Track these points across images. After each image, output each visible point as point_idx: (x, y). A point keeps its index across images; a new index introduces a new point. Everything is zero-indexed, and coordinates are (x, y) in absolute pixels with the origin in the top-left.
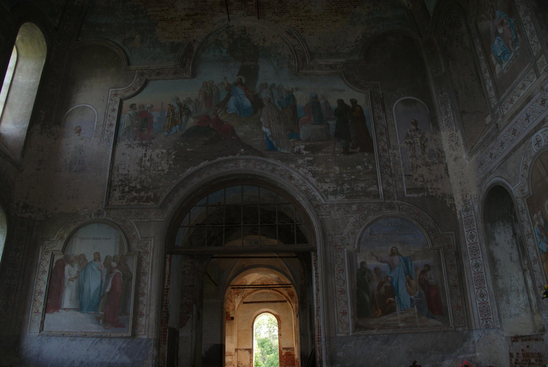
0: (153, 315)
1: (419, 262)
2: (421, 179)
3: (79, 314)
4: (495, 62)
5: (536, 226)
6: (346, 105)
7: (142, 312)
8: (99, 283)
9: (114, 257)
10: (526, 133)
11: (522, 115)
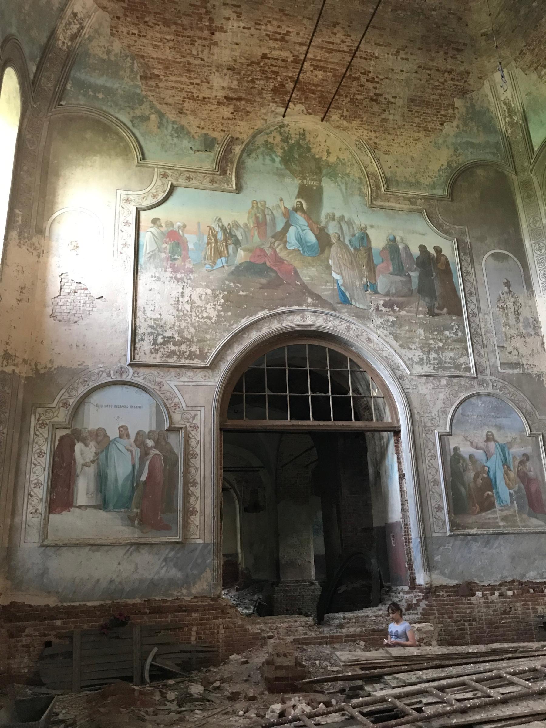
0: (209, 510)
1: (517, 450)
3: (102, 514)
6: (429, 253)
7: (194, 508)
8: (130, 468)
9: (149, 432)
10: (219, 345)
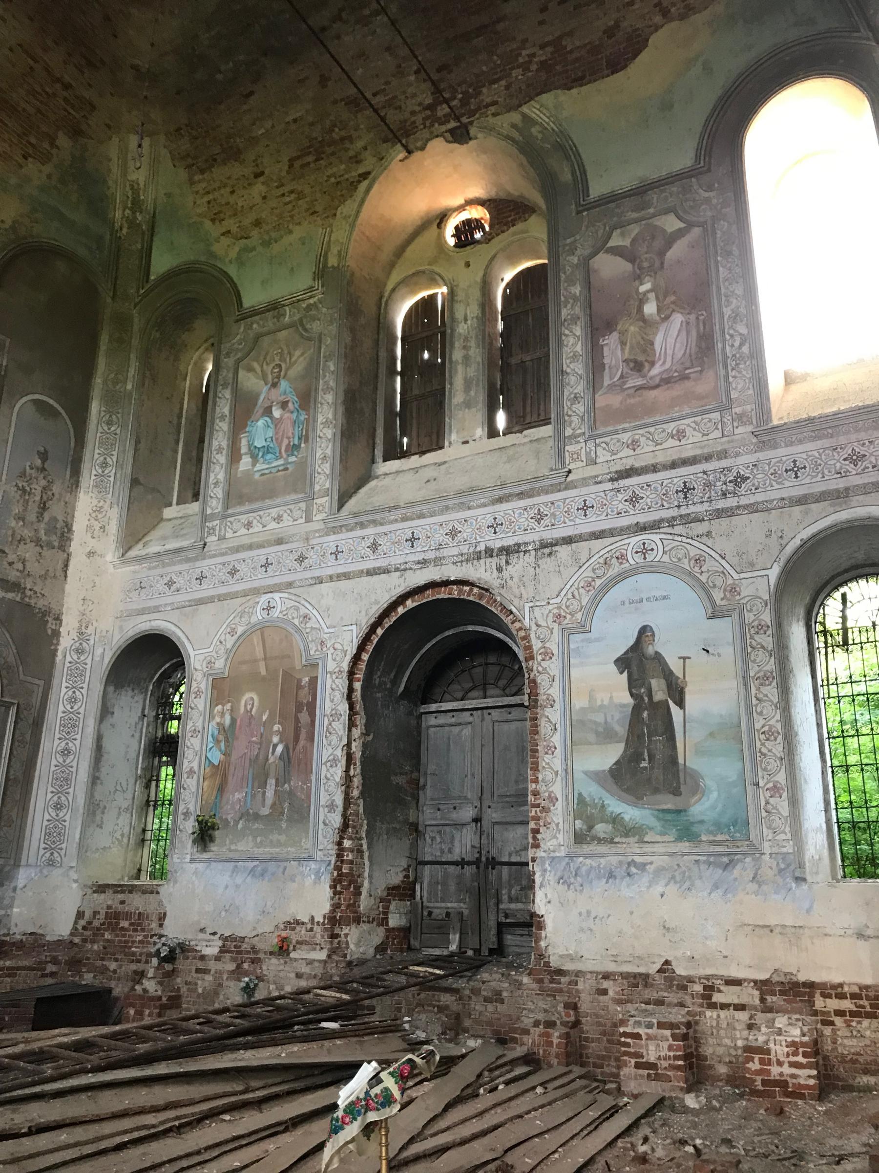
2: (20, 566)
4: (244, 450)
5: (213, 723)
10: (256, 584)
11: (260, 555)
